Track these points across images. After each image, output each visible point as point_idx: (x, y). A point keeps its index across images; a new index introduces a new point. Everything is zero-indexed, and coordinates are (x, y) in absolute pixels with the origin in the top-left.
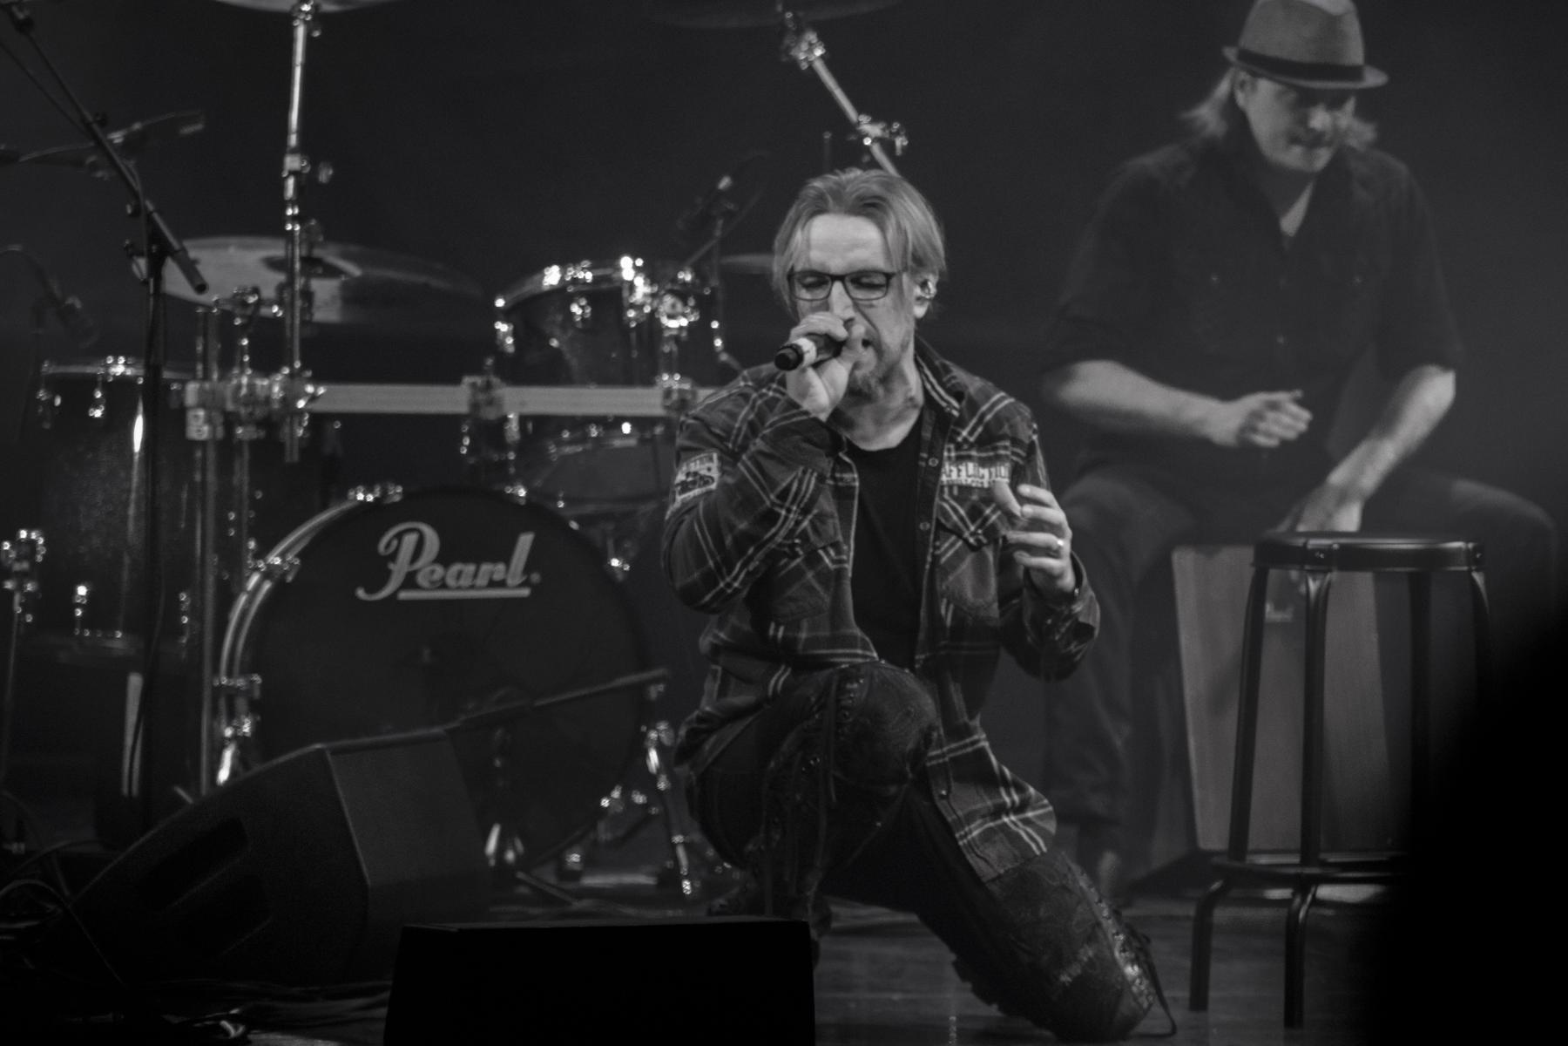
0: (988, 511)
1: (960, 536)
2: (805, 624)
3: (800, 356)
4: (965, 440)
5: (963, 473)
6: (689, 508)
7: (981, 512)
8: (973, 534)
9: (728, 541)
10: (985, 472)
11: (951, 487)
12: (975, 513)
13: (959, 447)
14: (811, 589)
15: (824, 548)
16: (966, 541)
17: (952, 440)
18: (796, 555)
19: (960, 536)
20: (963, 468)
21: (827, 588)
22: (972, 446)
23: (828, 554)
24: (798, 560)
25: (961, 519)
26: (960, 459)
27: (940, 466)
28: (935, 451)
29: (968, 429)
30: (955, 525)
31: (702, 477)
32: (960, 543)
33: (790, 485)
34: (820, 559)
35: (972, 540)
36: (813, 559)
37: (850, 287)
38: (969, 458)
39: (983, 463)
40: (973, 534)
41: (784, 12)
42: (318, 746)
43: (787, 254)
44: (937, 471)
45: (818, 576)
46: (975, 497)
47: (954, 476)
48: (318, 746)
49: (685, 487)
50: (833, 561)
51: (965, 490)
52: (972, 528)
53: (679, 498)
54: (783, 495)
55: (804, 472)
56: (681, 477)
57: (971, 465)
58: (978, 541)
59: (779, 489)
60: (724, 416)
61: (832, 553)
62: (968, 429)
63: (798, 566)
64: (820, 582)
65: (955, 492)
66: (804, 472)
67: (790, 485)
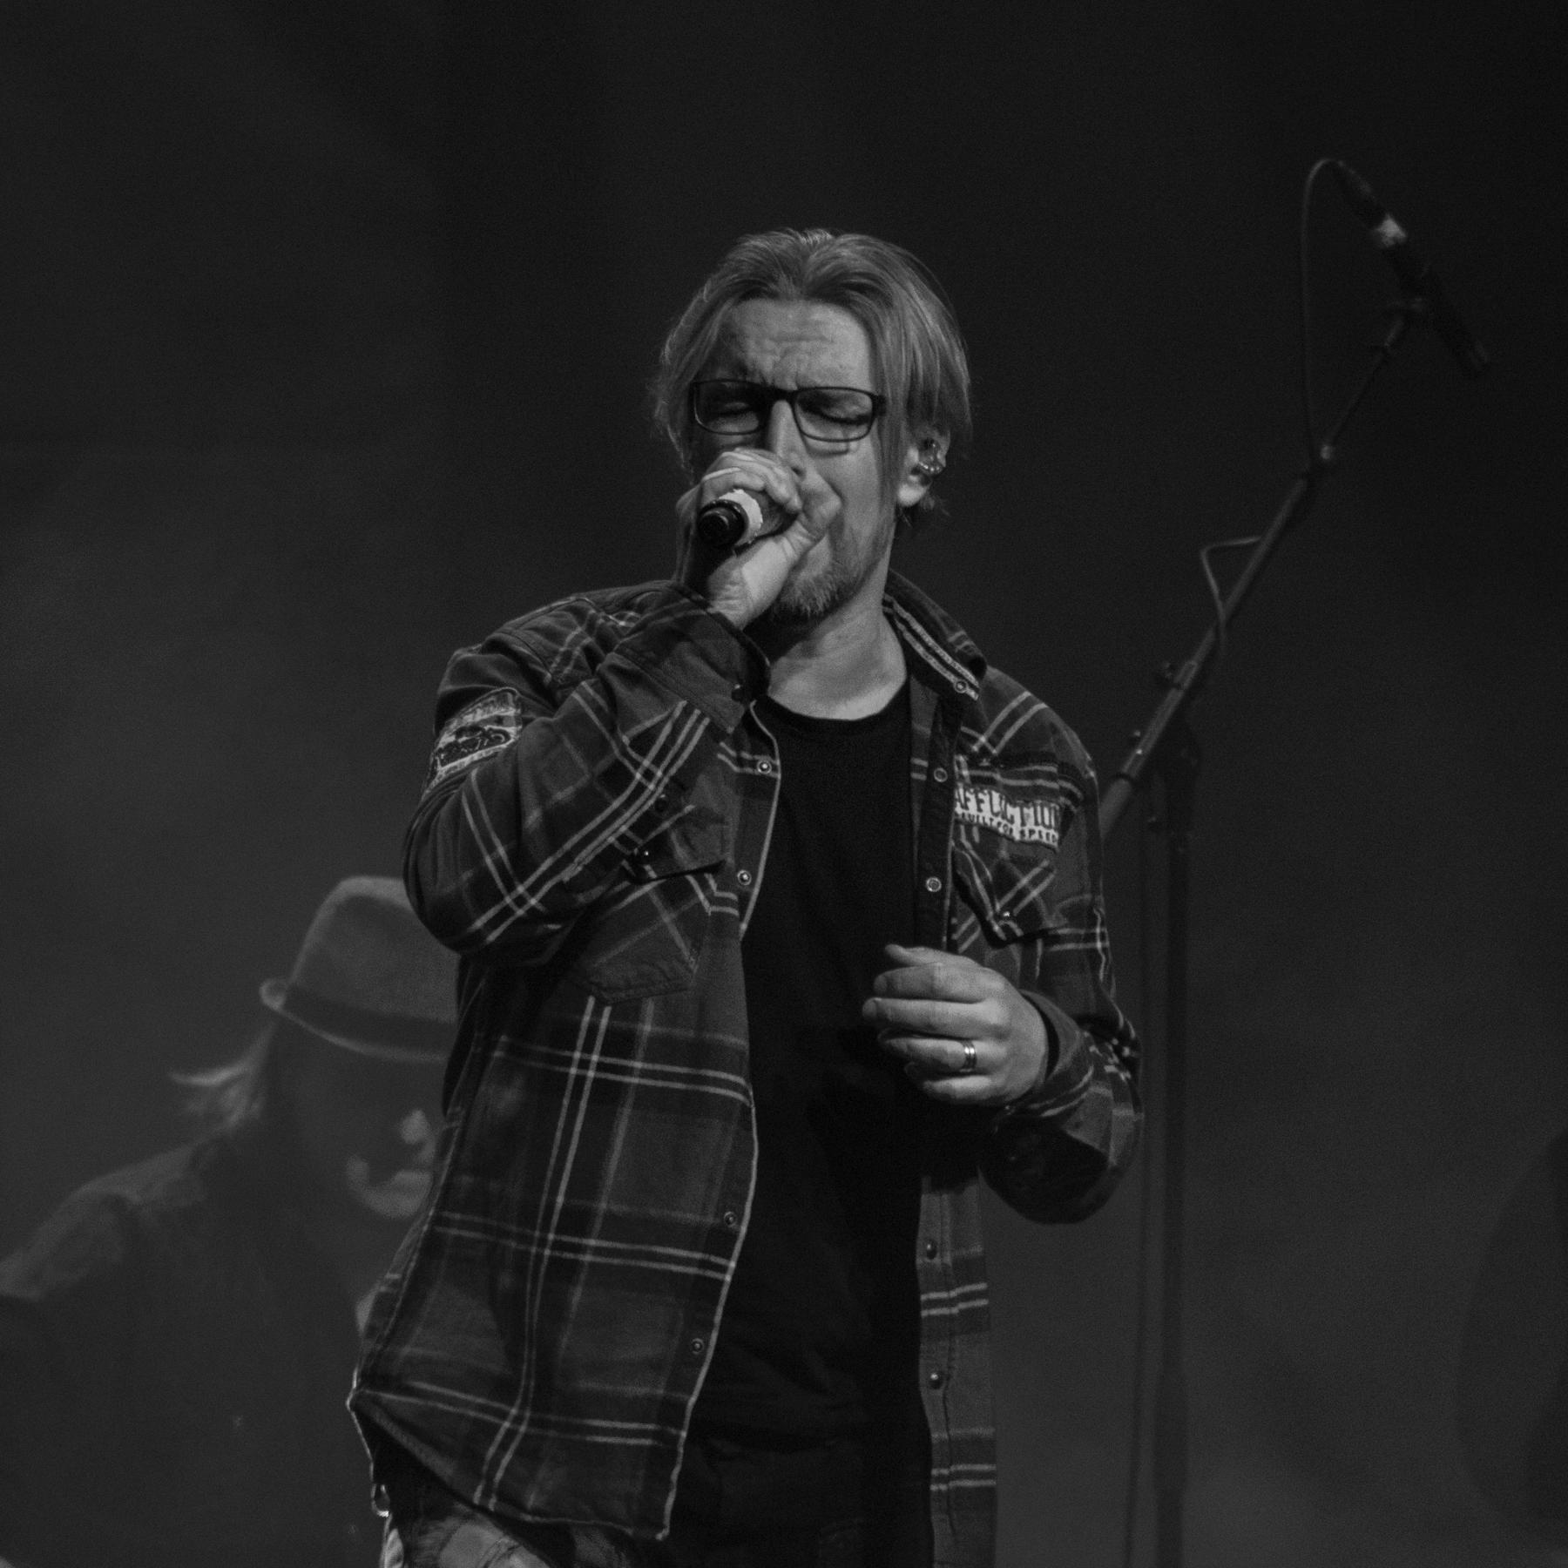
2: (650, 1008)
3: (740, 521)
4: (984, 750)
5: (985, 807)
6: (459, 779)
9: (533, 818)
10: (1014, 811)
11: (969, 826)
13: (973, 763)
15: (698, 873)
16: (987, 928)
17: (962, 750)
18: (641, 880)
20: (984, 797)
21: (696, 946)
22: (995, 763)
23: (704, 886)
24: (647, 888)
26: (979, 783)
27: (950, 786)
31: (486, 735)
33: (658, 728)
35: (996, 928)
36: (675, 890)
37: (798, 409)
38: (990, 783)
41: (931, 716)
42: (1319, 165)
45: (685, 921)
48: (1319, 165)
49: (453, 752)
53: (442, 771)
54: (643, 742)
55: (687, 712)
56: (447, 739)
59: (637, 729)
63: (645, 897)
64: (685, 934)
66: (687, 712)
67: (658, 728)
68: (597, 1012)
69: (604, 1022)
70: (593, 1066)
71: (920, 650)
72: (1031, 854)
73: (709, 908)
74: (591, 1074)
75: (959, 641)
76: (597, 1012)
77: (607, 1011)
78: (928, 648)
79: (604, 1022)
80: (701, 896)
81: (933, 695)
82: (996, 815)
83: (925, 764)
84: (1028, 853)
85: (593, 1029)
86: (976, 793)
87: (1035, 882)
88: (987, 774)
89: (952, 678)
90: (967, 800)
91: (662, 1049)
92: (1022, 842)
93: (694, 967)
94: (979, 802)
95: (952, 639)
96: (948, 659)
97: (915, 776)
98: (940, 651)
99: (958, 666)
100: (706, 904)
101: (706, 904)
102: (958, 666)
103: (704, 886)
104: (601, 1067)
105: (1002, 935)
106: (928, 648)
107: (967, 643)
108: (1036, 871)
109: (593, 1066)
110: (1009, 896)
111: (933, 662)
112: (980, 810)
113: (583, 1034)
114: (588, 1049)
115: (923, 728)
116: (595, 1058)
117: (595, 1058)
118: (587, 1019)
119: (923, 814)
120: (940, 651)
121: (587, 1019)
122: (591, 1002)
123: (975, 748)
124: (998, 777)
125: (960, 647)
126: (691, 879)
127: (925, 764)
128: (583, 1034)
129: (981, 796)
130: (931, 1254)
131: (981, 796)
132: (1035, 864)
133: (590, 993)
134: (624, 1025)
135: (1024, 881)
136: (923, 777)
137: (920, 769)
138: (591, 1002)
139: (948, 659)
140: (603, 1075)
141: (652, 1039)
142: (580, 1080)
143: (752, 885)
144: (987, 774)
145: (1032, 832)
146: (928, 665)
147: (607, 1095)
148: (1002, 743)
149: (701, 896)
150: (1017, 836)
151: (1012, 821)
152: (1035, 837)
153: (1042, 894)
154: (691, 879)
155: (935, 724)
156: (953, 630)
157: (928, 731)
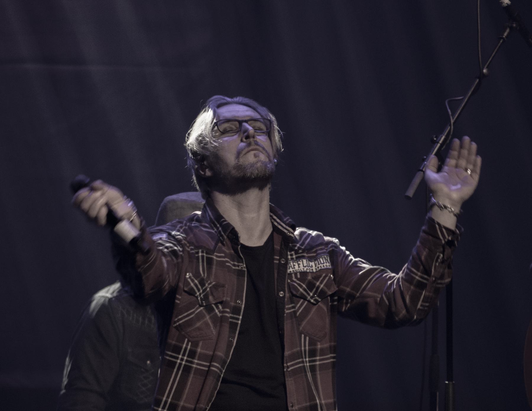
0: (318, 284)
1: (305, 299)
5: (301, 265)
7: (314, 285)
8: (312, 297)
10: (312, 264)
11: (296, 274)
12: (311, 286)
13: (297, 252)
14: (207, 324)
15: (216, 304)
16: (309, 301)
19: (305, 299)
21: (215, 326)
22: (304, 251)
23: (218, 307)
25: (305, 290)
26: (299, 258)
27: (287, 263)
28: (283, 255)
29: (319, 281)
30: (302, 294)
32: (306, 303)
34: (213, 310)
35: (312, 301)
38: (303, 257)
39: (310, 259)
40: (312, 297)
41: (281, 243)
43: (231, 248)
44: (285, 266)
46: (309, 278)
47: (297, 267)
50: (220, 312)
51: (304, 274)
52: (311, 294)
57: (305, 261)
58: (315, 300)
60: (104, 212)
61: (220, 307)
62: (319, 281)
65: (299, 276)
68: (187, 344)
69: (189, 347)
70: (184, 360)
71: (276, 224)
72: (318, 274)
73: (219, 315)
74: (184, 363)
75: (287, 220)
76: (187, 344)
77: (190, 344)
78: (278, 223)
79: (189, 347)
80: (217, 311)
81: (281, 237)
82: (305, 267)
83: (278, 258)
84: (317, 275)
85: (186, 349)
86: (297, 262)
87: (321, 283)
88: (302, 254)
89: (286, 231)
90: (294, 265)
91: (202, 357)
92: (316, 272)
93: (214, 333)
94: (299, 264)
95: (285, 220)
96: (284, 226)
97: (275, 262)
98: (282, 224)
99: (287, 227)
100: (218, 313)
101: (218, 313)
102: (287, 227)
103: (218, 307)
104: (187, 361)
105: (315, 302)
106: (278, 223)
107: (290, 220)
108: (321, 279)
109: (184, 360)
110: (314, 290)
111: (280, 227)
112: (299, 267)
113: (163, 403)
114: (184, 355)
115: (277, 247)
116: (185, 358)
117: (185, 358)
118: (164, 399)
119: (278, 273)
120: (282, 224)
121: (184, 346)
122: (186, 340)
123: (296, 248)
124: (305, 254)
125: (287, 222)
126: (213, 305)
127: (278, 258)
128: (163, 403)
129: (294, 264)
130: (292, 406)
131: (294, 264)
132: (320, 276)
133: (186, 338)
134: (194, 349)
135: (318, 284)
136: (278, 262)
137: (277, 260)
138: (186, 340)
139: (284, 226)
140: (187, 364)
141: (200, 354)
142: (184, 355)
143: (242, 304)
144: (302, 254)
145: (318, 267)
146: (279, 228)
147: (187, 369)
148: (305, 245)
149: (217, 311)
150: (314, 271)
151: (312, 267)
152: (320, 268)
153: (324, 285)
154: (213, 305)
155: (281, 245)
156: (286, 217)
157: (279, 248)
